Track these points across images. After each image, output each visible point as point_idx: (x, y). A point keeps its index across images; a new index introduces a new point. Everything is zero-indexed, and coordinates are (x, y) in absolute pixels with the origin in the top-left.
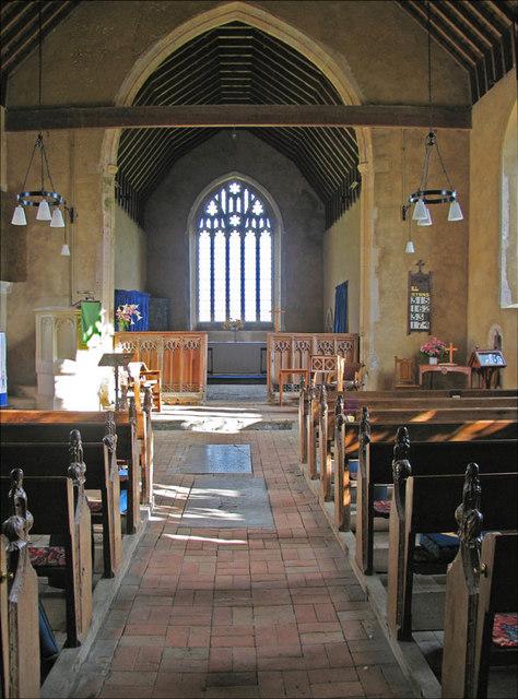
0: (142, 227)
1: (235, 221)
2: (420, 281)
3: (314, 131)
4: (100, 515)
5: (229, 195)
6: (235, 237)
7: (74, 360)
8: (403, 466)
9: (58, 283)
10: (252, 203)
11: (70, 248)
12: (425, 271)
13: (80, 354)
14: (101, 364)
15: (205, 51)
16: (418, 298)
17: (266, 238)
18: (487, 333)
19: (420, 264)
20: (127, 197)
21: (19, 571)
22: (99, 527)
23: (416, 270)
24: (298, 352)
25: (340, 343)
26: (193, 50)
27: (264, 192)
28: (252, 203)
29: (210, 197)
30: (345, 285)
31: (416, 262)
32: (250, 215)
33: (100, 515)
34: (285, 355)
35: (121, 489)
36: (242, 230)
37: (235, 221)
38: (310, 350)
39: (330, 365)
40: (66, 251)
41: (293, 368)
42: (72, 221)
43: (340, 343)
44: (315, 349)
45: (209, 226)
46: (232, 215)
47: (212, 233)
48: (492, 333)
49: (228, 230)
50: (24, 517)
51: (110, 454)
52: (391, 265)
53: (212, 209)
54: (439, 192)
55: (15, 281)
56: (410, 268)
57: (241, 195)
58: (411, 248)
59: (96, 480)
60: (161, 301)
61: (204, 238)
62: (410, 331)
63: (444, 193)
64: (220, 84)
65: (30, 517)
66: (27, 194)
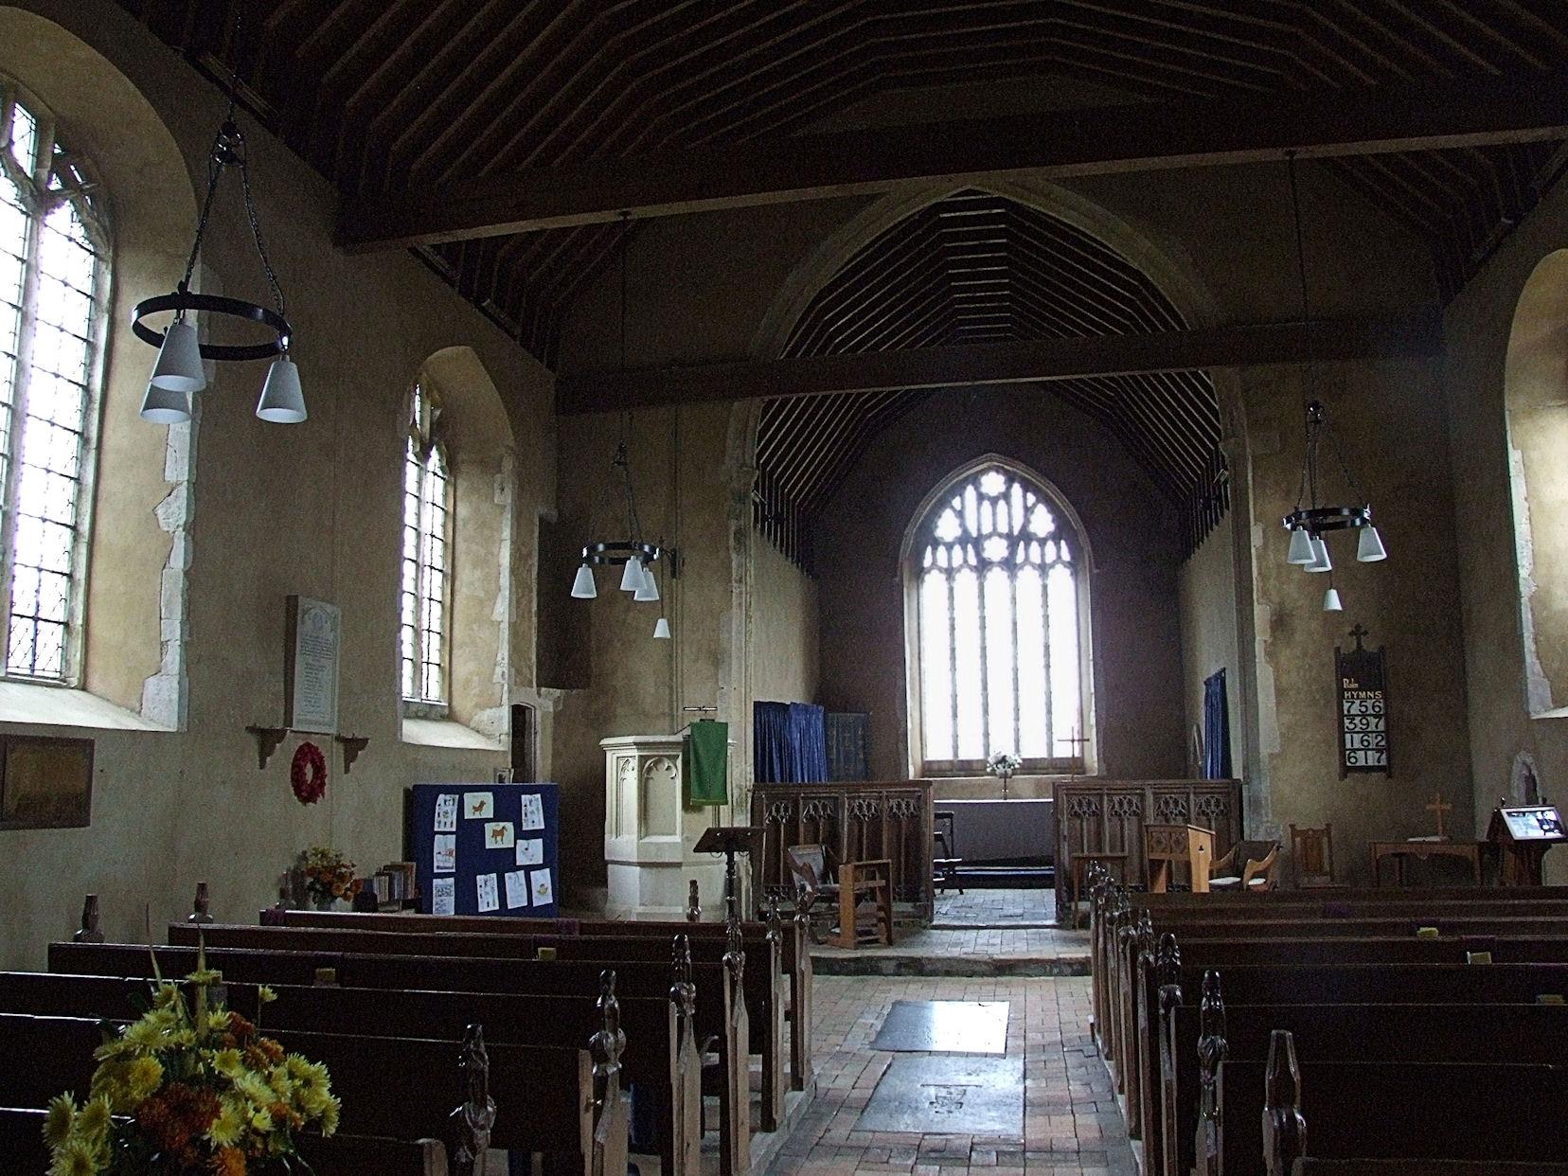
0: (816, 577)
1: (995, 549)
2: (1359, 668)
3: (1138, 382)
4: (715, 1081)
5: (981, 497)
6: (997, 577)
7: (758, 705)
8: (1171, 994)
9: (648, 687)
10: (1028, 510)
11: (670, 625)
12: (1370, 646)
13: (320, 799)
14: (366, 740)
15: (919, 240)
16: (1369, 703)
17: (1062, 581)
18: (1509, 773)
19: (1357, 632)
20: (779, 519)
21: (609, 1095)
22: (716, 1101)
23: (1350, 646)
24: (1115, 819)
25: (1203, 799)
26: (894, 241)
27: (1051, 490)
28: (1028, 510)
29: (943, 503)
30: (1220, 678)
31: (1348, 629)
32: (1026, 536)
33: (715, 1081)
34: (1088, 826)
35: (751, 1052)
36: (1010, 565)
37: (995, 549)
38: (1140, 816)
39: (1177, 842)
40: (661, 630)
41: (1108, 853)
42: (673, 575)
43: (1203, 799)
44: (1150, 812)
45: (943, 562)
46: (989, 536)
47: (950, 573)
48: (1518, 771)
49: (983, 566)
50: (616, 1034)
51: (733, 984)
52: (1298, 637)
53: (947, 526)
54: (1337, 512)
55: (571, 687)
56: (1337, 643)
57: (1006, 496)
58: (1334, 602)
59: (709, 1026)
60: (851, 717)
61: (933, 585)
62: (1346, 771)
63: (1346, 512)
64: (952, 304)
65: (621, 1034)
66: (601, 547)
